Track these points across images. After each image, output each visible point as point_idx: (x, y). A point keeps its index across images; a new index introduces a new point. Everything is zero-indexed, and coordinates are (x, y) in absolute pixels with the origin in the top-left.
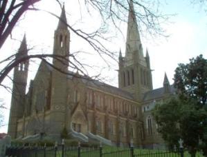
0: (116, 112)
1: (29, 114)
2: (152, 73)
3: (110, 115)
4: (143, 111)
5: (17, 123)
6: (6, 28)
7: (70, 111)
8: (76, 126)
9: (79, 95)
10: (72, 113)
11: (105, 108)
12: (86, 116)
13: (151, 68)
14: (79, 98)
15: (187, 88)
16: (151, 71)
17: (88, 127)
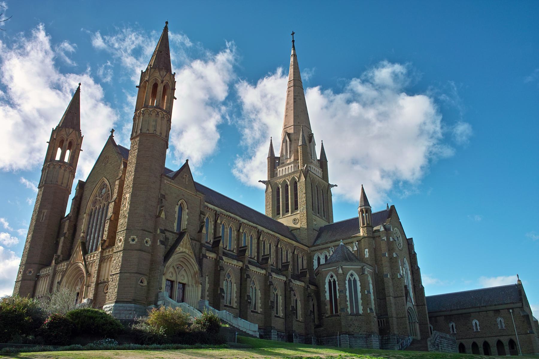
0: (241, 253)
1: (68, 255)
3: (253, 268)
4: (315, 263)
5: (38, 277)
7: (161, 250)
8: (176, 286)
9: (185, 217)
11: (241, 253)
12: (200, 263)
14: (184, 224)
15: (136, 23)
17: (203, 291)
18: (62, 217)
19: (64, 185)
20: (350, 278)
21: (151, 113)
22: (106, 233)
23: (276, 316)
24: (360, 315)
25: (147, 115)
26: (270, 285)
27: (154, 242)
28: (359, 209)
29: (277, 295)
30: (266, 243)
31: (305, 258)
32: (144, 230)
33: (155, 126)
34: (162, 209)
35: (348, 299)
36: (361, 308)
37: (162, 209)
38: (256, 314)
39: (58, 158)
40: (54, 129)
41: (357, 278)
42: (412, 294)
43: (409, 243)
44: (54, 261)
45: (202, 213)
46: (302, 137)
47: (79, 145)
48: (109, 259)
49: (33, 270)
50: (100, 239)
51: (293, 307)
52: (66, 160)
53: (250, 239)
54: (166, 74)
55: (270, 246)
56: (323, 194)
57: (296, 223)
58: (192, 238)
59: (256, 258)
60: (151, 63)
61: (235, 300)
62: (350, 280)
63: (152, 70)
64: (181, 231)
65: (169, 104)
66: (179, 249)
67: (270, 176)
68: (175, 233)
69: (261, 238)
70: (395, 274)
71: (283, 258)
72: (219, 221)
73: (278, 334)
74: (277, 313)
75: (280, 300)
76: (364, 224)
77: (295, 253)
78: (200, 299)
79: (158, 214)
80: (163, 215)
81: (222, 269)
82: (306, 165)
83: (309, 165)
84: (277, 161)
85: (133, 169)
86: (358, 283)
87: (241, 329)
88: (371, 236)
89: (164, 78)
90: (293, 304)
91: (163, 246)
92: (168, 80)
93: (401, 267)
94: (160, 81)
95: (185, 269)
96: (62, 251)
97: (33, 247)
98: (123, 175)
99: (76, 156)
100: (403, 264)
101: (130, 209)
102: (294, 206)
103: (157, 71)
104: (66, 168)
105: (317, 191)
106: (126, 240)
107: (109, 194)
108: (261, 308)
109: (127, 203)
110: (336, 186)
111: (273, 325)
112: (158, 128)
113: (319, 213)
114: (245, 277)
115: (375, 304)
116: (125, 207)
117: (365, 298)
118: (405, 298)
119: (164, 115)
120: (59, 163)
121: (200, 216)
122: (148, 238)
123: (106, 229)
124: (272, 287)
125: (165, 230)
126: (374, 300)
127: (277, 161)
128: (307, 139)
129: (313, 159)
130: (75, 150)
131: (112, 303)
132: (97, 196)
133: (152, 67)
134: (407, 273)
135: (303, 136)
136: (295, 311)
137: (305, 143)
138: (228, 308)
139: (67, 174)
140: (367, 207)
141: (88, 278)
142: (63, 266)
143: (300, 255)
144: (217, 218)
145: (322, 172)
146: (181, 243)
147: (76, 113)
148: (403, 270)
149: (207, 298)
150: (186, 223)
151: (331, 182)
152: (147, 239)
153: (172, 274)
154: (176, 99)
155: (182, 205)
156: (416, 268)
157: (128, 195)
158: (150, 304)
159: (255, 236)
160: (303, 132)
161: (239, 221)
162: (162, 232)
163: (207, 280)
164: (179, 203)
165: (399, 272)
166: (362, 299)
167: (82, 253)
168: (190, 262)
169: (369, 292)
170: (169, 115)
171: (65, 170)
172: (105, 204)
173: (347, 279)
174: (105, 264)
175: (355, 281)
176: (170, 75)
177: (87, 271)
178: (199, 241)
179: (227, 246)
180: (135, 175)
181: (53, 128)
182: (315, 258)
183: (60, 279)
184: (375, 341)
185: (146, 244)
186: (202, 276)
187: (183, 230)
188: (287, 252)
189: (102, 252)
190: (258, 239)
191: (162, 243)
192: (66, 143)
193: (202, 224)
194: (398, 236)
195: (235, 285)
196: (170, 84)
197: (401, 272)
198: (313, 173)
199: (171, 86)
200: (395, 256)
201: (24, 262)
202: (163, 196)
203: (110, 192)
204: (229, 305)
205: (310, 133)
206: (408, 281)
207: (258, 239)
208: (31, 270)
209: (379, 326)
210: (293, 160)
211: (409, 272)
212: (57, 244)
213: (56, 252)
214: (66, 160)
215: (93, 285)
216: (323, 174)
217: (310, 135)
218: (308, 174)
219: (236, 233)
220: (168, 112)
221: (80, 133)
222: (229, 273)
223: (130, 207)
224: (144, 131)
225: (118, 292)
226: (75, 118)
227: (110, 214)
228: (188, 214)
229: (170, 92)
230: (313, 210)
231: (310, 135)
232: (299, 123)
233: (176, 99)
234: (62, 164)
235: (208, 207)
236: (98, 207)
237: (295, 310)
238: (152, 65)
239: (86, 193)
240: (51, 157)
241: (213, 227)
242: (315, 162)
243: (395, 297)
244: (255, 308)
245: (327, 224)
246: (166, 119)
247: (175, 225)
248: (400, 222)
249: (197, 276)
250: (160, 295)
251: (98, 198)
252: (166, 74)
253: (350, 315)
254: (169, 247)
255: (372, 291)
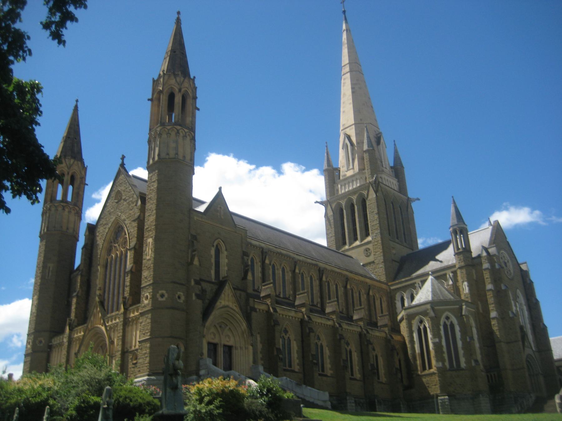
2: (414, 205)
6: (345, 51)
7: (198, 306)
8: (220, 350)
9: (224, 261)
10: (206, 314)
13: (411, 194)
16: (409, 200)
18: (71, 270)
19: (71, 231)
20: (445, 323)
21: (170, 132)
22: (127, 289)
23: (351, 379)
24: (463, 369)
25: (164, 136)
26: (340, 339)
27: (188, 296)
28: (451, 229)
29: (350, 352)
30: (330, 284)
31: (384, 299)
32: (175, 283)
33: (176, 149)
34: (194, 253)
35: (445, 349)
36: (463, 360)
37: (195, 255)
38: (324, 378)
39: (59, 197)
41: (455, 322)
42: (530, 337)
43: (524, 275)
44: (67, 328)
45: (245, 254)
46: (367, 140)
47: (83, 178)
48: (135, 322)
50: (121, 297)
51: (372, 365)
52: (69, 199)
53: (309, 281)
54: (184, 80)
55: (337, 288)
56: (401, 212)
57: (369, 254)
58: (235, 287)
59: (319, 305)
60: (164, 68)
61: (297, 361)
62: (445, 326)
63: (166, 77)
64: (221, 279)
65: (191, 118)
66: (221, 303)
67: (328, 194)
68: (212, 283)
69: (324, 279)
71: (355, 302)
72: (267, 261)
73: (355, 401)
74: (352, 375)
75: (355, 357)
77: (371, 293)
78: (251, 364)
79: (189, 260)
80: (196, 262)
81: (277, 323)
82: (375, 176)
83: (379, 175)
85: (154, 207)
86: (457, 328)
87: (307, 399)
89: (181, 85)
90: (372, 361)
91: (200, 302)
92: (187, 88)
93: (513, 302)
94: (177, 90)
95: (230, 328)
96: (76, 314)
98: (142, 214)
99: (81, 193)
100: (516, 298)
101: (154, 258)
102: (364, 232)
103: (172, 77)
104: (70, 209)
105: (394, 208)
106: (154, 298)
107: (126, 238)
108: (330, 369)
109: (150, 250)
110: (418, 199)
111: (348, 390)
112: (181, 151)
113: (397, 238)
114: (307, 331)
115: (481, 354)
116: (149, 253)
117: (468, 347)
118: (521, 343)
119: (186, 133)
120: (62, 204)
121: (243, 258)
122: (179, 291)
123: (128, 283)
124: (342, 341)
125: (201, 280)
126: (480, 348)
127: (337, 174)
128: (373, 140)
129: (384, 166)
130: (79, 188)
131: (144, 376)
132: (111, 242)
133: (165, 72)
134: (522, 310)
135: (368, 137)
136: (376, 371)
137: (372, 146)
138: (288, 373)
139: (72, 218)
140: (462, 226)
141: (111, 346)
142: (79, 334)
143: (377, 295)
144: (264, 257)
145: (398, 183)
146: (223, 295)
147: (76, 139)
148: (516, 306)
149: (260, 362)
150: (226, 268)
151: (411, 194)
152: (179, 293)
153: (214, 335)
154: (198, 109)
155: (219, 247)
156: (529, 282)
157: (150, 240)
158: (190, 374)
159: (315, 276)
160: (368, 132)
161: (293, 258)
162: (197, 282)
163: (259, 339)
164: (215, 244)
165: (511, 309)
166: (463, 348)
167: (100, 315)
168: (235, 318)
169: (472, 338)
170: (193, 132)
171: (70, 212)
172: (122, 252)
173: (442, 323)
174: (130, 328)
175: (452, 325)
176: (189, 81)
177: (110, 338)
178: (244, 290)
179: (280, 293)
180: (157, 213)
182: (397, 298)
183: (77, 348)
184: (485, 401)
185: (178, 299)
186: (252, 335)
187: (223, 278)
188: (360, 294)
189: (125, 313)
190: (321, 279)
191: (198, 296)
192: (67, 178)
193: (247, 268)
194: (506, 261)
195: (295, 342)
196: (190, 92)
197: (514, 308)
198: (386, 185)
199: (191, 95)
200: (503, 288)
201: (33, 331)
202: (194, 237)
203: (127, 236)
204: (289, 368)
205: (377, 133)
206: (525, 319)
207: (321, 279)
209: (489, 381)
210: (358, 170)
211: (525, 308)
212: (69, 305)
213: (69, 315)
214: (69, 199)
215: (118, 354)
216: (399, 186)
217: (377, 135)
218: (379, 187)
219: (290, 275)
220: (190, 128)
221: (83, 163)
222: (285, 328)
223: (155, 255)
224: (163, 155)
225: (150, 363)
226: (76, 145)
227: (129, 265)
228: (227, 257)
229: (191, 102)
230: (390, 235)
231: (379, 134)
232: (361, 120)
233: (198, 109)
234: (64, 204)
235: (251, 244)
236: (113, 256)
237: (375, 370)
240: (52, 197)
241: (260, 269)
242: (388, 170)
243: (508, 343)
244: (323, 371)
245: (410, 251)
246: (188, 138)
247: (213, 272)
248: (508, 242)
249: (245, 335)
250: (202, 362)
252: (184, 80)
253: (449, 370)
254: (207, 301)
255: (475, 336)
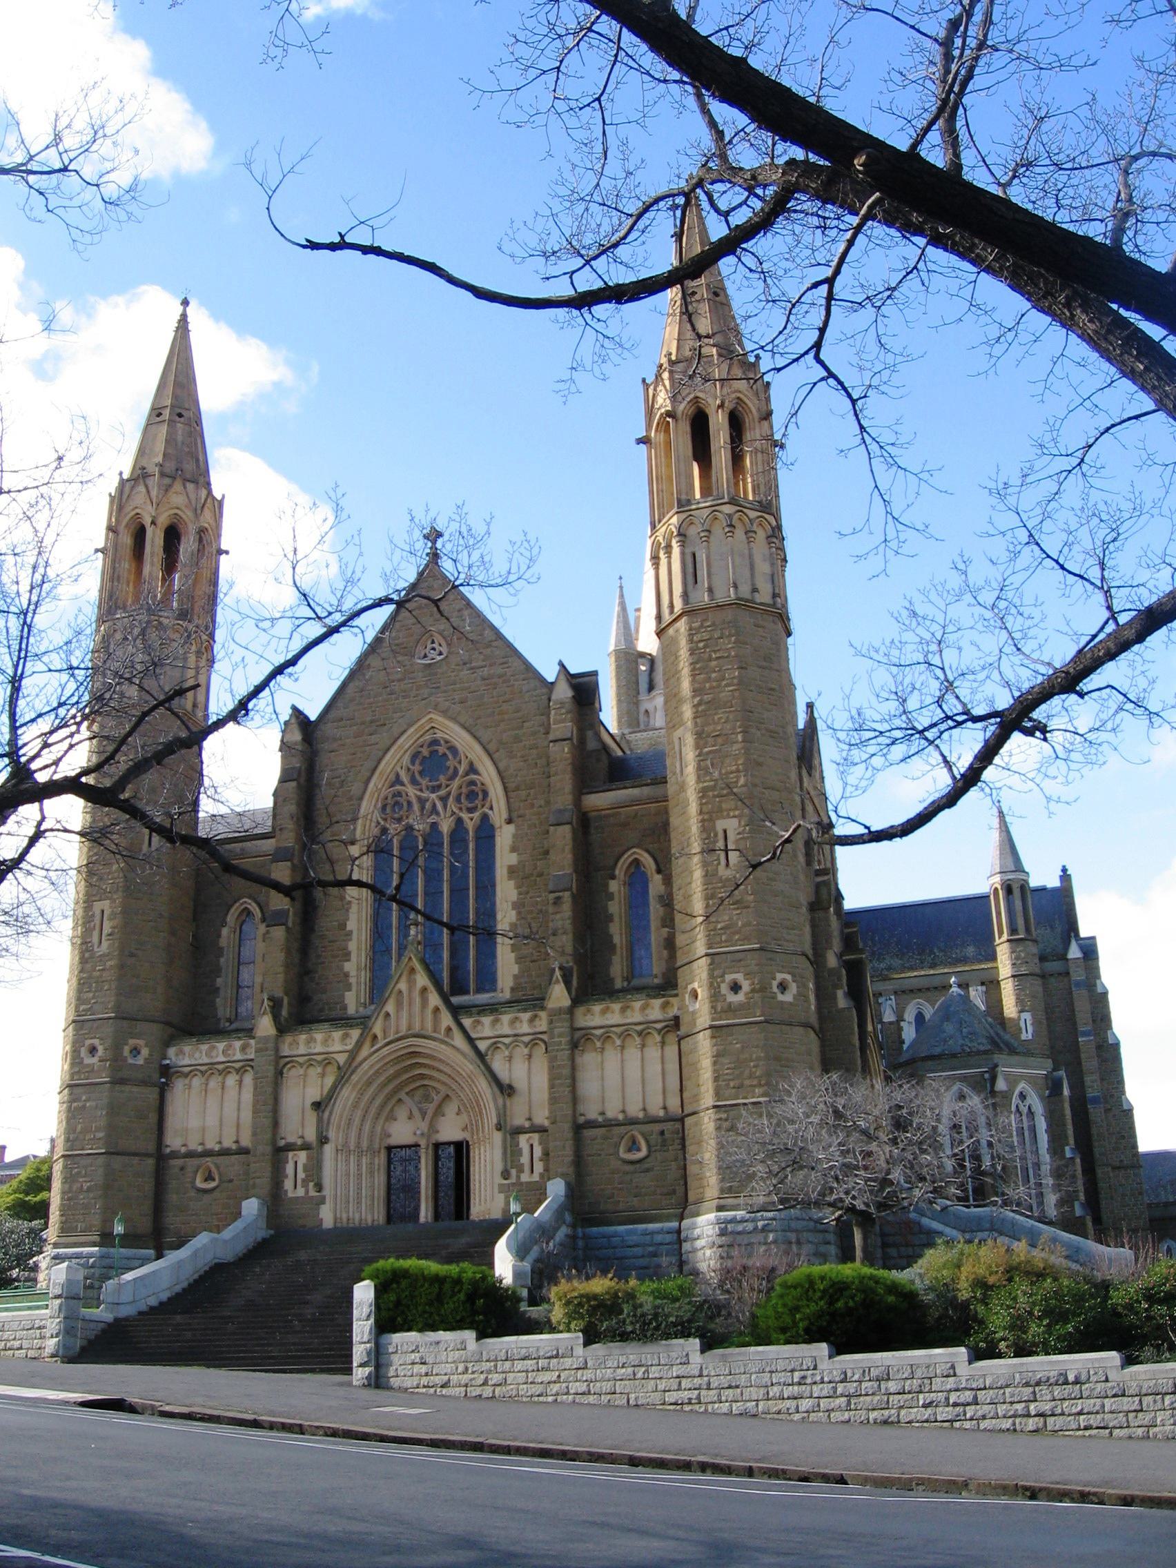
5: (167, 1072)
40: (125, 476)
41: (1039, 1108)
49: (146, 1045)
70: (1112, 1096)
76: (1013, 931)
84: (643, 668)
88: (1037, 971)
97: (132, 955)
127: (643, 668)
133: (673, 358)
181: (121, 474)
208: (141, 1042)
238: (674, 351)
239: (333, 763)
251: (411, 791)
